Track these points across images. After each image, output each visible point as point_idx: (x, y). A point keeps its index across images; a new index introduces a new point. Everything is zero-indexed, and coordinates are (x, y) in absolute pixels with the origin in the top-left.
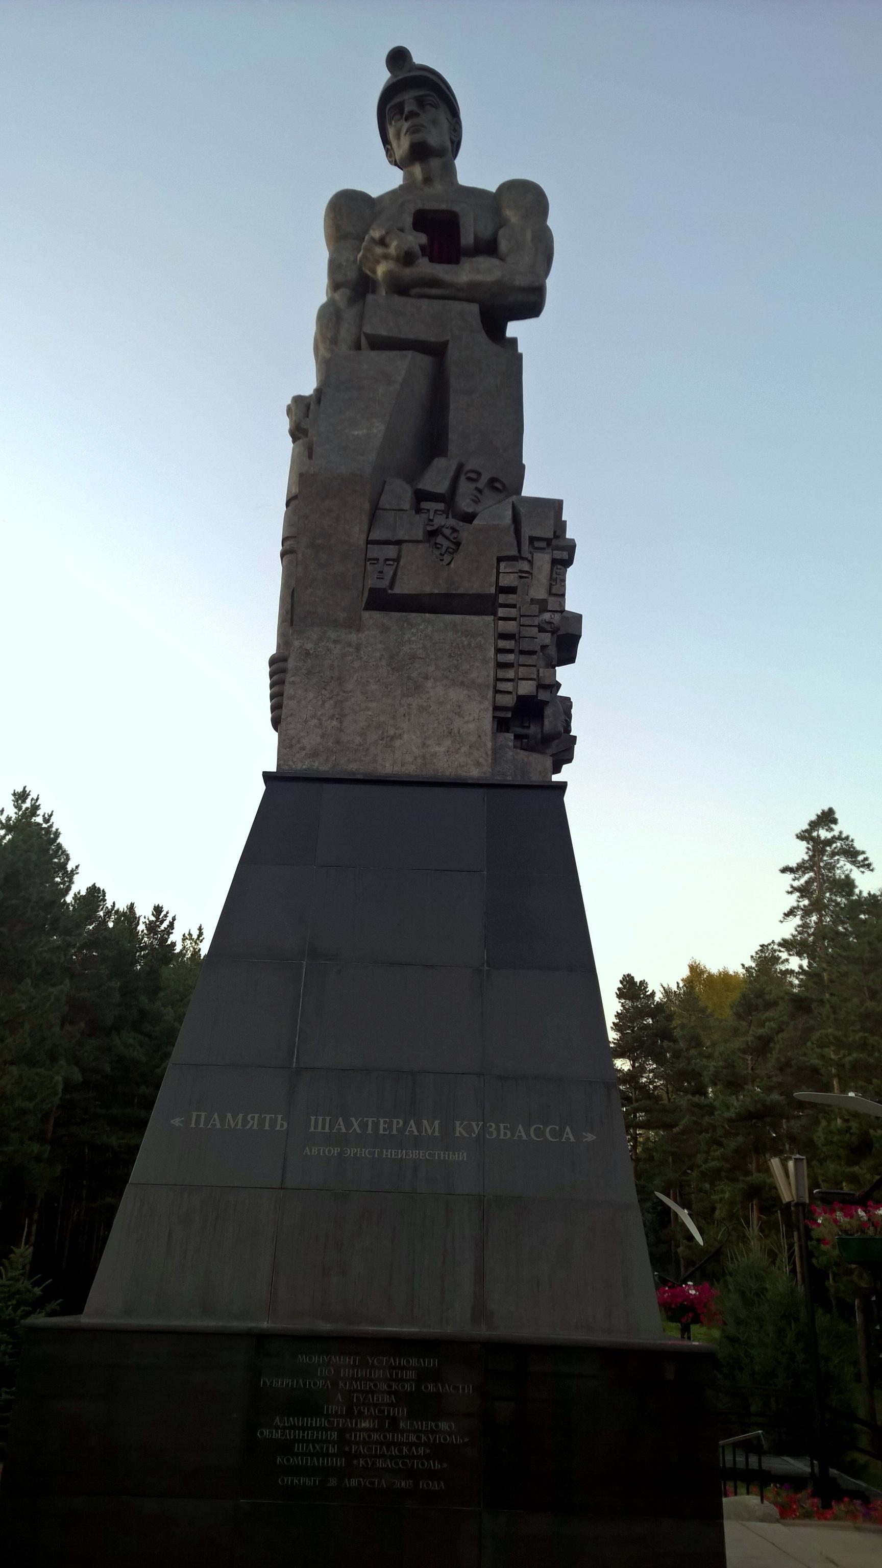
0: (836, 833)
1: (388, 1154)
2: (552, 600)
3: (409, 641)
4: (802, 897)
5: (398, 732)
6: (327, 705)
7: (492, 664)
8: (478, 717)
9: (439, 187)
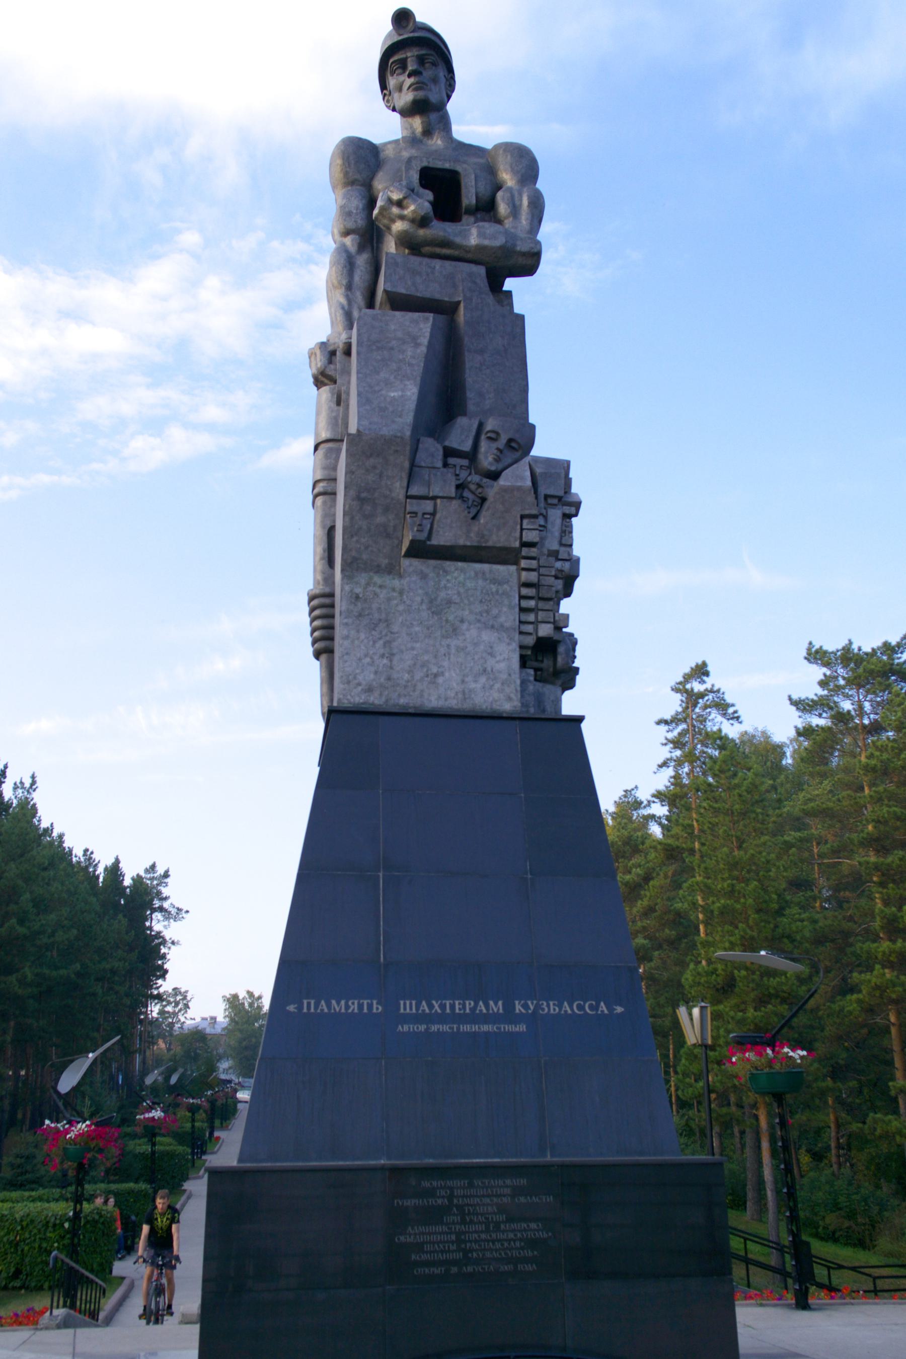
0: (708, 686)
1: (466, 1028)
2: (562, 549)
3: (445, 587)
4: (675, 748)
5: (440, 670)
7: (517, 610)
8: (506, 658)
9: (437, 142)
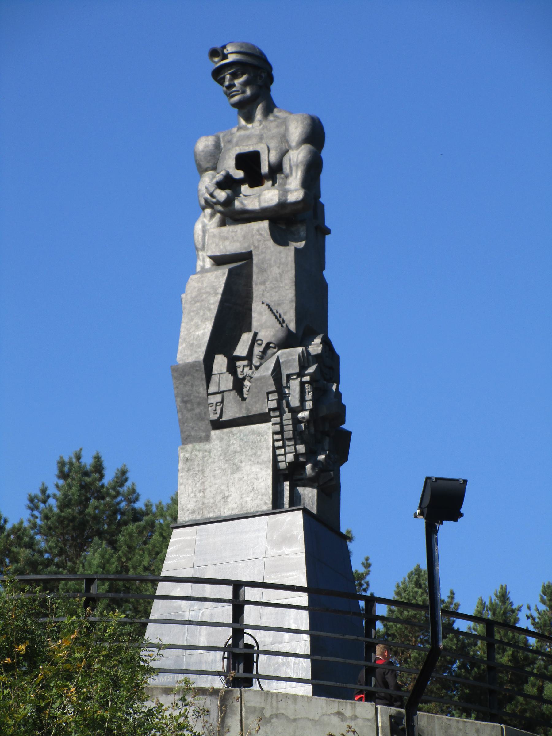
3: (233, 444)
5: (230, 494)
6: (197, 486)
